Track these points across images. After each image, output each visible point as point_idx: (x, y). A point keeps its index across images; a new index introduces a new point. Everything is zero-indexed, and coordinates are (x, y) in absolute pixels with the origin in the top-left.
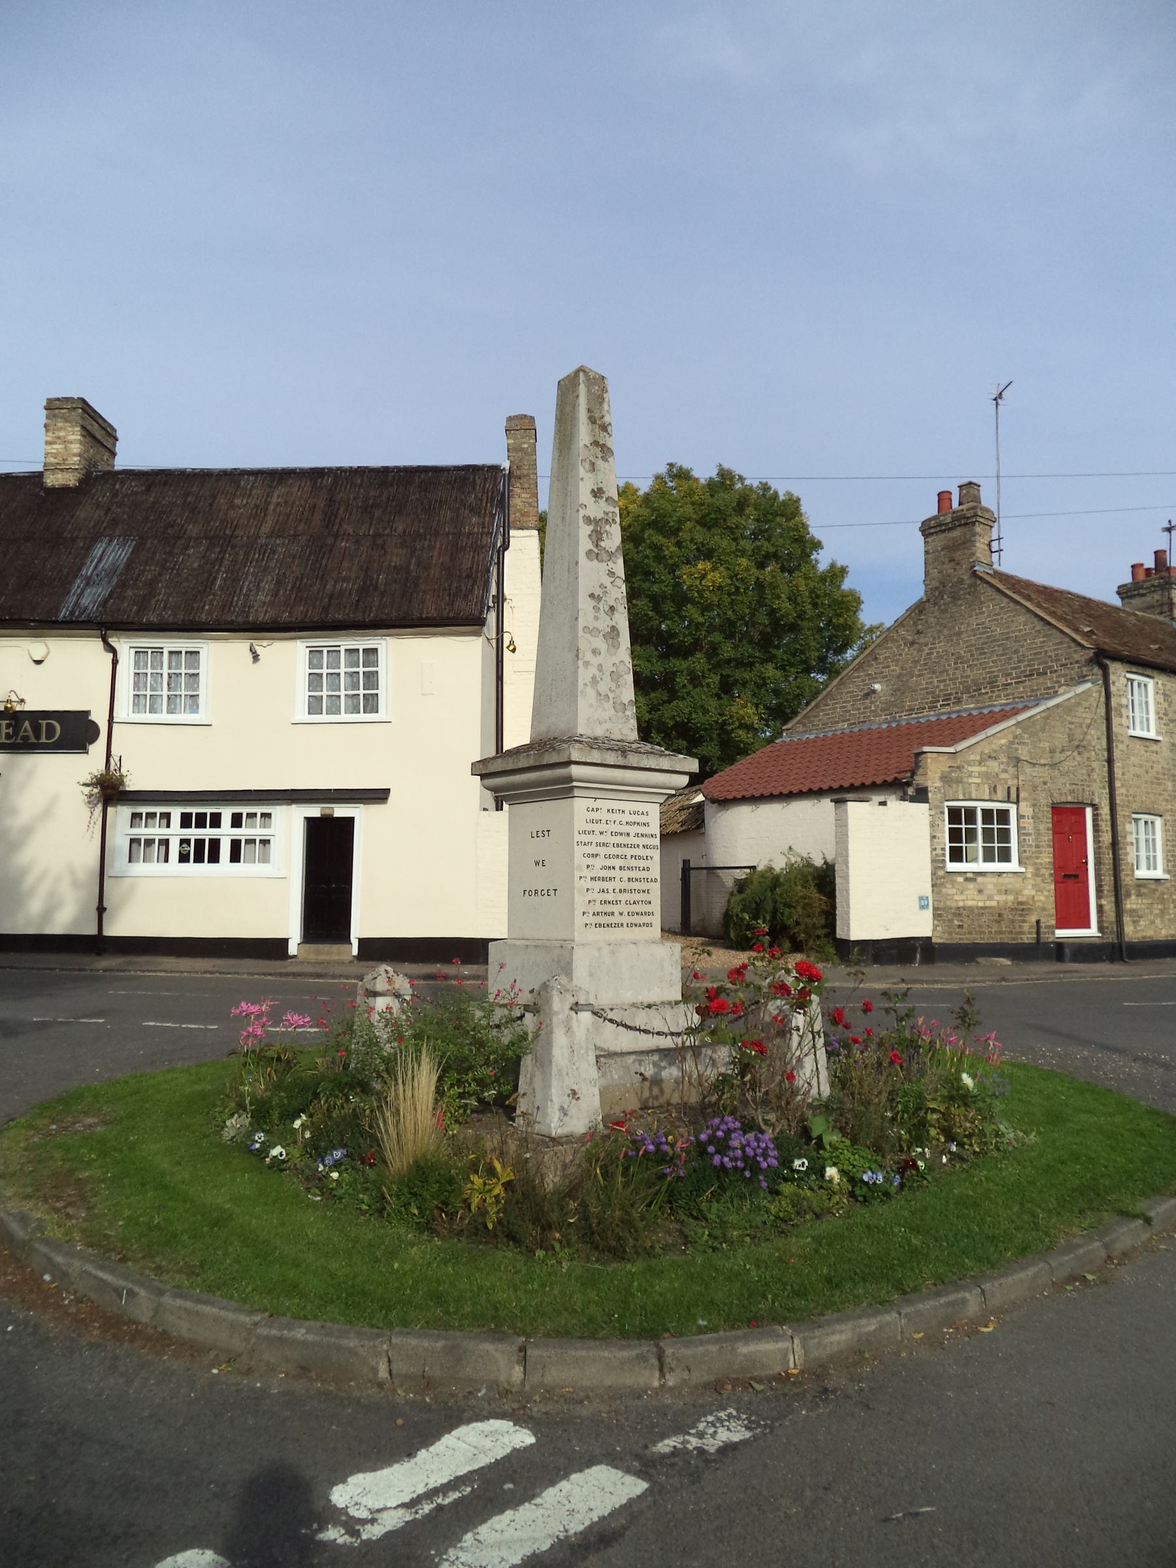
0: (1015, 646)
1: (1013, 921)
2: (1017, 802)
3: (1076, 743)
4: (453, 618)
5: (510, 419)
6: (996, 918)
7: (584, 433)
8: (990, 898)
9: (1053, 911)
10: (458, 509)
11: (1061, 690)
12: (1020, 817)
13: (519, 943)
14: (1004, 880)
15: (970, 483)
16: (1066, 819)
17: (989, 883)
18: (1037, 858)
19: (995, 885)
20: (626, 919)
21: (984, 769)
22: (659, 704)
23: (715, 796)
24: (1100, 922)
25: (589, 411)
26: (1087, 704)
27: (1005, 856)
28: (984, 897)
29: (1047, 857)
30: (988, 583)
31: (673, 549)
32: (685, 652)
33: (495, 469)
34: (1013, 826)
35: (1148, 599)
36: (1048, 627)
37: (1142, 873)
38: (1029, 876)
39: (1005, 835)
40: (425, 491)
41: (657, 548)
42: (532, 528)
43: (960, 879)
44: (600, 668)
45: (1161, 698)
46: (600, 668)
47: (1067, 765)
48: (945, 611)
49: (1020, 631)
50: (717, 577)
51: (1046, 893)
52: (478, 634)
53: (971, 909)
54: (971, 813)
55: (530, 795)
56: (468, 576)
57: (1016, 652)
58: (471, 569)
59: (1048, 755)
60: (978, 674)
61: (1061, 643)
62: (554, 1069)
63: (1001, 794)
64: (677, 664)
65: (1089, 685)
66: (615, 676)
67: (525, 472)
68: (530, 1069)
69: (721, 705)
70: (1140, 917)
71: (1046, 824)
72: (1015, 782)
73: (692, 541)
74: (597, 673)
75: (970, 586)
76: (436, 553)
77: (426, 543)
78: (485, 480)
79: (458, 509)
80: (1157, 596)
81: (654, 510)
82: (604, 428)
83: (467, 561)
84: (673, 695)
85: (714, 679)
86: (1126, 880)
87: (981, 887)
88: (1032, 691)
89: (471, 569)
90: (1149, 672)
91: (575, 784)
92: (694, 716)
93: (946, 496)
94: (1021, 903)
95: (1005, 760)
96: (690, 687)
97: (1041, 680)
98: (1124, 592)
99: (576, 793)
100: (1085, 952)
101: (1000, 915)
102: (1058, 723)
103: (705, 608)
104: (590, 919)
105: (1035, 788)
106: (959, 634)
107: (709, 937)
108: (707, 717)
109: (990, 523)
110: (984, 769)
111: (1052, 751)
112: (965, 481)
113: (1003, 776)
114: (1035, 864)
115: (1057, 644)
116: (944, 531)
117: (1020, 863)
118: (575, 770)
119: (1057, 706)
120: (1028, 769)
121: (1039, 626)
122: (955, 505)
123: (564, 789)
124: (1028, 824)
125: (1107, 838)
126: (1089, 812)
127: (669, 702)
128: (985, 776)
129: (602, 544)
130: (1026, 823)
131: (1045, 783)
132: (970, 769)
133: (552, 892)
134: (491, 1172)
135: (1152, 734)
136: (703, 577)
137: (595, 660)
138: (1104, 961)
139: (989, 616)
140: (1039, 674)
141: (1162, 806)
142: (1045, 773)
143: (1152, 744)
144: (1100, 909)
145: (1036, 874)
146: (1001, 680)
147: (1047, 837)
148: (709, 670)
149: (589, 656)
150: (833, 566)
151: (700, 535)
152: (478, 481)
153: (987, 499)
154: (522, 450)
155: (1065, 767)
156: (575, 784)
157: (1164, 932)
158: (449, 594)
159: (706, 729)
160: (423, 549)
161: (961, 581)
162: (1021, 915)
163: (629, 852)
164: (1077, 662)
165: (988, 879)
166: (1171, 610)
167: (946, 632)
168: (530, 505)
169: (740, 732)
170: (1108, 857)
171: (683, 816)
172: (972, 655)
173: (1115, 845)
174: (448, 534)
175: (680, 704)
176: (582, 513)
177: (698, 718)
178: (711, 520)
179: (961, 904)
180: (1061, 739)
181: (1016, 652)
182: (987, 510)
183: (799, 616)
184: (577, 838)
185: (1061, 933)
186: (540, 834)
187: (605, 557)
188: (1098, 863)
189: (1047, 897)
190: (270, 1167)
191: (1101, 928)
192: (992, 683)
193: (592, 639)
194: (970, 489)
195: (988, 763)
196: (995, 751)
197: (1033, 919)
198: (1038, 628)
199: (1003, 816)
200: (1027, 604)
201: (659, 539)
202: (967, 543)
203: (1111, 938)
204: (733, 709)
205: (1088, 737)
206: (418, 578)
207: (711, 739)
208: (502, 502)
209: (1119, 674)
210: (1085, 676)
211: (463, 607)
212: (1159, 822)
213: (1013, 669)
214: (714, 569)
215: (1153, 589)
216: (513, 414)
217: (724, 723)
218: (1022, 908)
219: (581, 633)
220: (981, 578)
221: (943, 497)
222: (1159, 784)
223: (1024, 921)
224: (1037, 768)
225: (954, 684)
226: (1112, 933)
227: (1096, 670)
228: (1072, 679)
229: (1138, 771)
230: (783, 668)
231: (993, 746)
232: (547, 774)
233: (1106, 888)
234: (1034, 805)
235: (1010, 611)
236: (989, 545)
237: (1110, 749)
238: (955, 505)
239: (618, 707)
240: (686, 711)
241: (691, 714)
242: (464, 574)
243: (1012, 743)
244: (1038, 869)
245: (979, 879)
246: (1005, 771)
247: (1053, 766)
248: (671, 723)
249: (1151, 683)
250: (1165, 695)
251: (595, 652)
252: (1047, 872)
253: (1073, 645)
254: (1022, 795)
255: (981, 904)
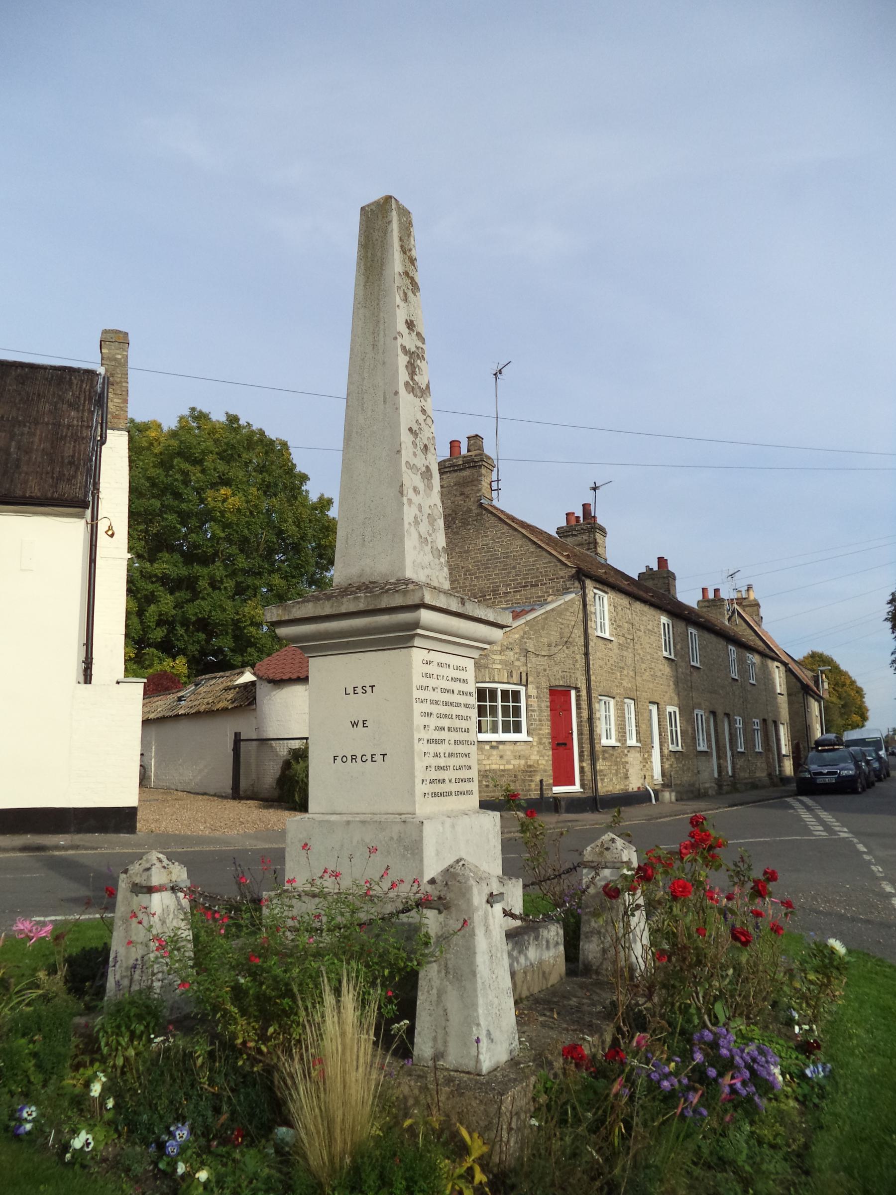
0: (513, 563)
1: (524, 781)
2: (526, 686)
3: (565, 640)
4: (57, 499)
5: (105, 332)
6: (513, 778)
7: (397, 264)
8: (508, 762)
9: (551, 772)
10: (56, 403)
11: (549, 599)
12: (528, 697)
13: (333, 818)
14: (519, 747)
15: (477, 436)
16: (558, 697)
17: (507, 749)
18: (540, 729)
19: (512, 752)
20: (454, 787)
21: (504, 657)
22: (183, 602)
23: (271, 676)
24: (582, 780)
25: (401, 240)
26: (572, 610)
27: (517, 729)
28: (504, 762)
29: (546, 730)
30: (491, 513)
31: (199, 475)
32: (206, 561)
33: (91, 373)
34: (523, 704)
35: (579, 538)
36: (538, 550)
37: (605, 742)
38: (535, 744)
39: (517, 711)
40: (23, 384)
41: (185, 474)
42: (122, 429)
43: (487, 747)
44: (420, 507)
45: (612, 608)
46: (420, 507)
47: (560, 657)
48: (457, 533)
49: (517, 552)
50: (235, 501)
51: (546, 758)
52: (81, 516)
53: (494, 771)
54: (493, 692)
55: (348, 645)
56: (70, 463)
57: (514, 568)
58: (73, 457)
59: (546, 648)
60: (483, 583)
61: (550, 562)
62: (479, 981)
63: (515, 679)
64: (198, 569)
65: (573, 595)
66: (431, 518)
67: (118, 380)
68: (436, 983)
69: (235, 606)
70: (605, 776)
71: (546, 703)
72: (525, 668)
73: (215, 469)
74: (418, 513)
75: (478, 515)
76: (36, 440)
77: (26, 430)
78: (82, 381)
79: (56, 403)
80: (585, 537)
81: (181, 442)
82: (412, 261)
83: (68, 449)
84: (196, 595)
85: (230, 584)
86: (598, 748)
87: (502, 754)
88: (526, 599)
89: (73, 457)
90: (605, 589)
91: (419, 631)
92: (213, 613)
93: (456, 444)
94: (530, 766)
95: (517, 650)
96: (210, 590)
97: (534, 590)
98: (560, 531)
99: (417, 642)
100: (575, 805)
101: (515, 776)
102: (553, 624)
103: (226, 526)
104: (428, 788)
105: (538, 674)
106: (468, 551)
107: (261, 800)
108: (225, 615)
109: (491, 468)
110: (504, 657)
111: (549, 645)
112: (472, 434)
113: (517, 663)
114: (539, 734)
115: (547, 563)
116: (456, 471)
117: (528, 734)
118: (426, 616)
119: (553, 610)
120: (534, 659)
121: (532, 548)
122: (464, 451)
123: (402, 637)
124: (533, 701)
125: (585, 714)
126: (573, 693)
127: (192, 600)
128: (503, 663)
129: (416, 378)
130: (533, 703)
131: (545, 670)
132: (494, 657)
133: (379, 758)
134: (463, 1150)
135: (607, 635)
136: (224, 501)
137: (416, 499)
138: (587, 811)
139: (492, 539)
140: (532, 586)
141: (615, 691)
142: (544, 662)
143: (608, 643)
144: (582, 769)
145: (540, 743)
146: (503, 589)
147: (547, 713)
148: (226, 576)
149: (411, 494)
150: (321, 498)
151: (222, 466)
152: (75, 382)
153: (489, 449)
154: (116, 360)
155: (558, 658)
156: (419, 631)
157: (618, 787)
158: (53, 478)
159: (222, 625)
160: (22, 434)
161: (470, 511)
162: (530, 776)
163: (456, 711)
164: (562, 578)
165: (508, 747)
166: (596, 547)
167: (457, 550)
168: (121, 409)
169: (252, 629)
170: (586, 730)
171: (231, 695)
172: (479, 569)
173: (591, 719)
174: (47, 424)
175: (202, 603)
176: (400, 341)
177: (217, 616)
178: (229, 454)
179: (488, 768)
180: (554, 637)
181: (514, 568)
182: (490, 458)
183: (302, 538)
184: (417, 694)
185: (557, 789)
186: (359, 690)
187: (419, 394)
188: (580, 733)
189: (547, 761)
190: (71, 1163)
191: (583, 785)
192: (495, 591)
193: (413, 476)
194: (475, 440)
195: (506, 653)
196: (511, 644)
197: (538, 779)
198: (531, 550)
199: (516, 695)
200: (524, 531)
201: (186, 466)
202: (475, 481)
203: (589, 793)
204: (246, 609)
205: (573, 635)
206: (18, 460)
207: (227, 633)
208: (101, 401)
209: (591, 589)
210: (568, 589)
211: (65, 489)
212: (612, 702)
213: (511, 581)
214: (234, 495)
215: (583, 531)
216: (108, 328)
217: (239, 621)
218: (530, 770)
219: (404, 468)
220: (486, 509)
221: (454, 445)
222: (613, 673)
223: (532, 781)
224: (539, 658)
225: (464, 591)
226: (590, 789)
227: (577, 584)
228: (558, 590)
229: (601, 663)
230: (285, 578)
231: (510, 640)
232: (384, 619)
233: (586, 753)
234: (538, 688)
235: (510, 536)
236: (491, 485)
237: (586, 645)
238: (464, 451)
239: (435, 552)
240: (207, 609)
241: (210, 612)
242: (66, 461)
243: (522, 637)
244: (540, 739)
245: (501, 747)
246: (518, 660)
247: (550, 656)
248: (193, 619)
249: (606, 597)
250: (615, 607)
251: (416, 490)
252: (547, 741)
253: (559, 564)
254: (529, 679)
255: (502, 767)
